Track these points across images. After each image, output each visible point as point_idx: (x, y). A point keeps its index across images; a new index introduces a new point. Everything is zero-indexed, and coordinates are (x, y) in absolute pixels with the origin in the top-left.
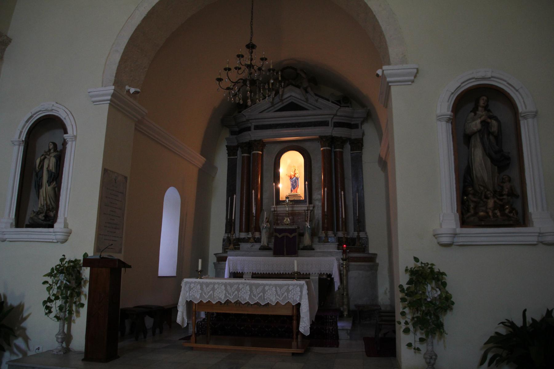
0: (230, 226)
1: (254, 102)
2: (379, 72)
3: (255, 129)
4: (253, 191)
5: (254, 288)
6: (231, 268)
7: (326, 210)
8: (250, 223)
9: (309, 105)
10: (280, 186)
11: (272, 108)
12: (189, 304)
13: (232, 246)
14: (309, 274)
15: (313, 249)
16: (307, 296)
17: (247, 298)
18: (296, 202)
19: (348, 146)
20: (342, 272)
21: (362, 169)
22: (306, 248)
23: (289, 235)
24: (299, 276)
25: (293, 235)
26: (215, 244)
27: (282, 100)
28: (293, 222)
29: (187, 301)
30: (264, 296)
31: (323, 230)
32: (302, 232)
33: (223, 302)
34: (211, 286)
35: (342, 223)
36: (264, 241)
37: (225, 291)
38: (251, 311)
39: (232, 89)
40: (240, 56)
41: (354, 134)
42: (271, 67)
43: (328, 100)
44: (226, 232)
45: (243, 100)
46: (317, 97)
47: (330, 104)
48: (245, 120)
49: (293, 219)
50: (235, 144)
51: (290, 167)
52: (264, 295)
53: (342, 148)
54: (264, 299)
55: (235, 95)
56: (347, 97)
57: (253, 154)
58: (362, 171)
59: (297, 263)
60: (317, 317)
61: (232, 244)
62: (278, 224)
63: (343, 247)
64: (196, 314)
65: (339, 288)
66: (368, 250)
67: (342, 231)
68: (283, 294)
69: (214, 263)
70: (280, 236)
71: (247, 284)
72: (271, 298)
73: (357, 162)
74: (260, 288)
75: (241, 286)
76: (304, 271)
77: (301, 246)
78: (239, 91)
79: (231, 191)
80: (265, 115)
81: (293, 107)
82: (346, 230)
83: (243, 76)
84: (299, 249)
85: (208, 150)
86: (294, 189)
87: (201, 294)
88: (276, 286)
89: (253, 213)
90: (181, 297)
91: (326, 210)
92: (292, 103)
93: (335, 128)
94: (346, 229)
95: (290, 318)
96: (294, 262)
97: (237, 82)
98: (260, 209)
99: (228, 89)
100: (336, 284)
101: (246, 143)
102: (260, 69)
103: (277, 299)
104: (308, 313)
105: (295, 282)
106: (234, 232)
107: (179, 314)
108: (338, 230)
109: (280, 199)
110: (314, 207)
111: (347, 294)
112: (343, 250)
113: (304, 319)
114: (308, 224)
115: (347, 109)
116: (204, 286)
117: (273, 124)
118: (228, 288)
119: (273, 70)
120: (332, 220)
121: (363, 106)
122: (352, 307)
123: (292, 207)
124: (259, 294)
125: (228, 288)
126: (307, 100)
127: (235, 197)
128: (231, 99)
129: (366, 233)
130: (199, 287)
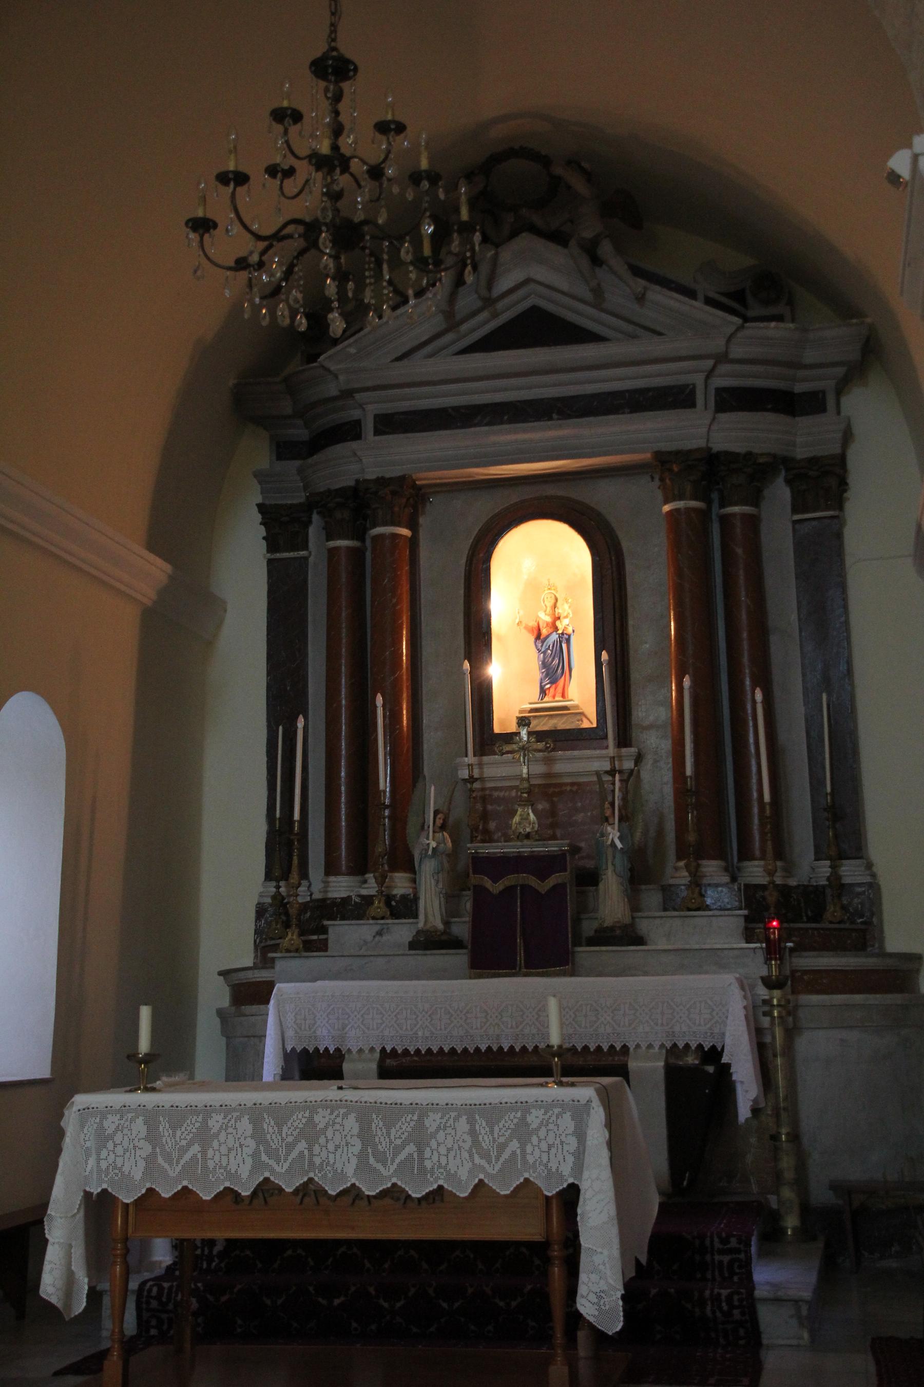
0: (284, 847)
1: (355, 315)
2: (900, 163)
3: (377, 432)
4: (379, 700)
5: (377, 1123)
6: (290, 1033)
7: (689, 771)
8: (371, 835)
9: (604, 316)
10: (497, 671)
11: (449, 337)
12: (98, 1207)
13: (292, 937)
14: (625, 1048)
15: (639, 941)
16: (605, 1154)
17: (350, 1170)
18: (562, 739)
19: (780, 493)
20: (768, 1039)
21: (843, 586)
22: (605, 937)
23: (533, 881)
24: (576, 1064)
25: (552, 881)
26: (225, 931)
27: (489, 302)
28: (553, 826)
29: (87, 1195)
30: (421, 1159)
31: (679, 858)
32: (590, 864)
33: (245, 1193)
34: (193, 1124)
35: (762, 825)
36: (431, 911)
37: (252, 1143)
38: (367, 1229)
39: (261, 265)
40: (286, 116)
41: (807, 437)
42: (424, 164)
43: (690, 293)
44: (269, 876)
45: (308, 316)
46: (643, 282)
47: (697, 309)
48: (334, 392)
49: (553, 813)
50: (299, 498)
51: (532, 588)
52: (421, 1152)
53: (755, 499)
54: (423, 1170)
55: (275, 292)
56: (775, 275)
57: (377, 538)
58: (845, 600)
59: (561, 1008)
60: (657, 1242)
61: (294, 926)
62: (488, 838)
63: (767, 929)
64: (127, 1251)
65: (756, 1111)
66: (882, 941)
67: (763, 858)
68: (502, 1147)
69: (220, 1013)
70: (495, 888)
71: (350, 1107)
72: (452, 1168)
73: (822, 562)
74: (405, 1126)
75: (322, 1118)
76: (601, 1033)
77: (588, 928)
78: (288, 274)
79: (285, 701)
80: (422, 367)
81: (538, 328)
82: (779, 854)
83: (310, 204)
84: (577, 943)
85: (178, 527)
86: (554, 681)
87: (150, 1160)
88: (470, 1111)
89: (378, 793)
90: (59, 1180)
91: (689, 771)
92: (534, 309)
93: (724, 417)
94: (780, 849)
95: (539, 1249)
96: (542, 1010)
97: (278, 237)
98: (409, 771)
99: (241, 264)
100: (740, 1090)
101: (341, 492)
102: (376, 173)
103: (475, 1168)
104: (614, 1231)
105: (552, 1092)
106: (304, 875)
107: (53, 1256)
108: (745, 854)
109: (497, 729)
110: (639, 759)
111: (795, 1137)
112: (768, 940)
113: (598, 1259)
114: (613, 834)
115: (773, 329)
116: (164, 1127)
117: (456, 409)
118: (268, 1125)
119: (433, 178)
120: (719, 811)
121: (845, 310)
122: (821, 1195)
123: (549, 761)
124: (398, 1150)
125: (268, 1125)
126: (598, 297)
127: (301, 723)
128: (256, 309)
129: (869, 866)
130: (140, 1127)
